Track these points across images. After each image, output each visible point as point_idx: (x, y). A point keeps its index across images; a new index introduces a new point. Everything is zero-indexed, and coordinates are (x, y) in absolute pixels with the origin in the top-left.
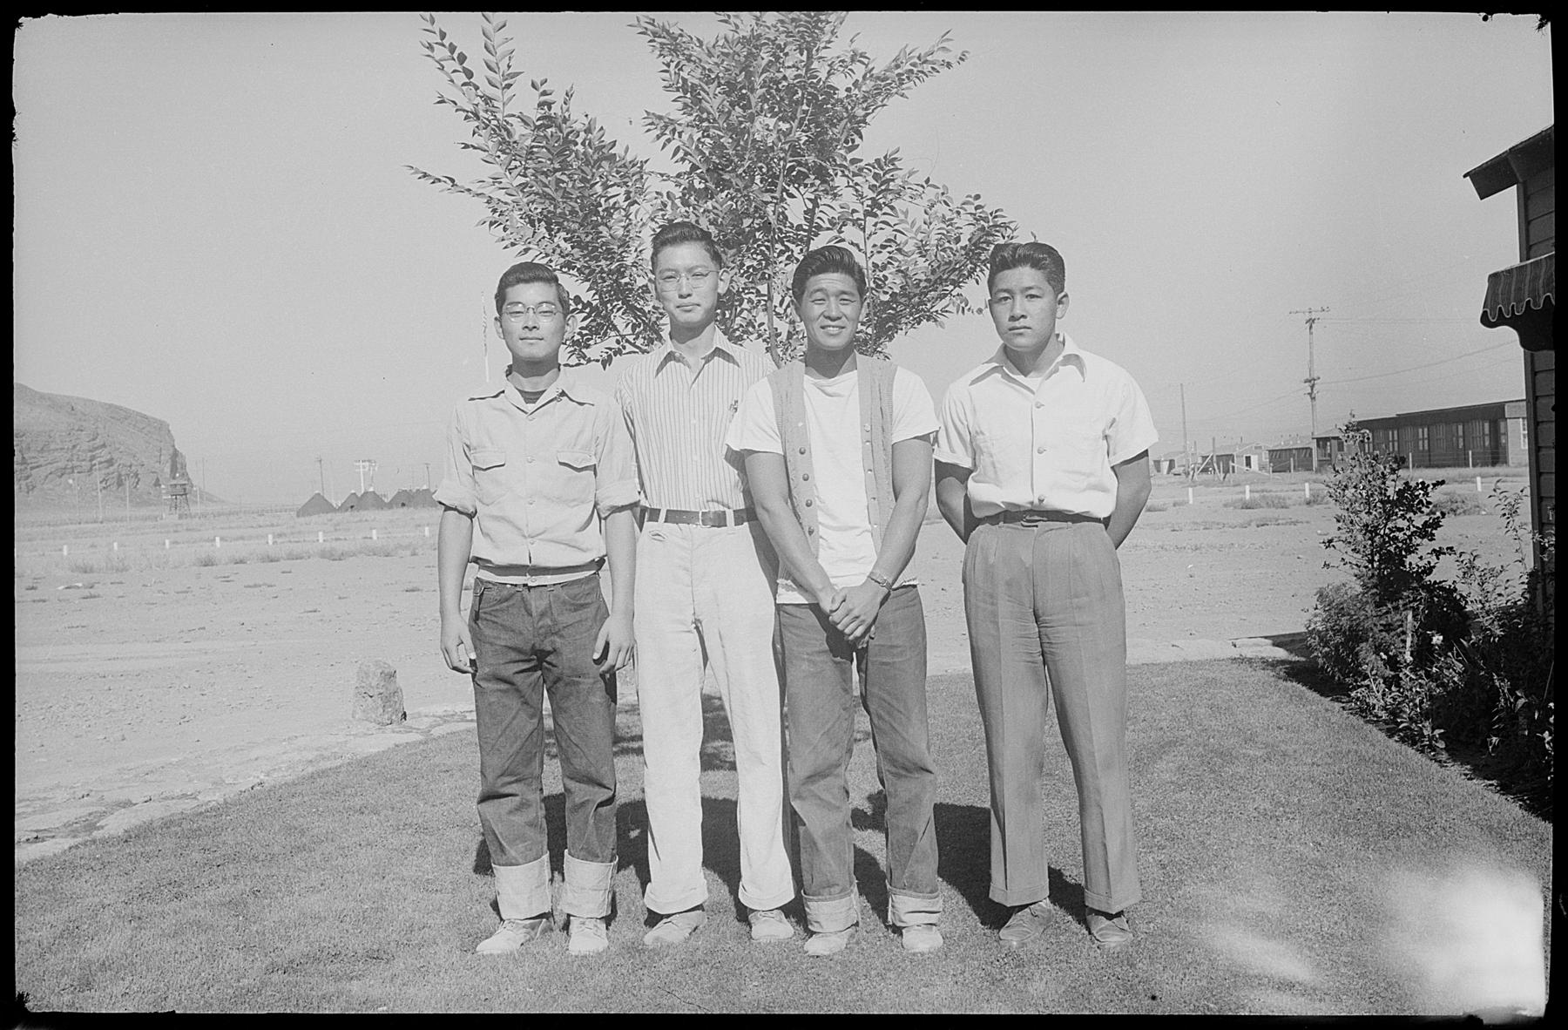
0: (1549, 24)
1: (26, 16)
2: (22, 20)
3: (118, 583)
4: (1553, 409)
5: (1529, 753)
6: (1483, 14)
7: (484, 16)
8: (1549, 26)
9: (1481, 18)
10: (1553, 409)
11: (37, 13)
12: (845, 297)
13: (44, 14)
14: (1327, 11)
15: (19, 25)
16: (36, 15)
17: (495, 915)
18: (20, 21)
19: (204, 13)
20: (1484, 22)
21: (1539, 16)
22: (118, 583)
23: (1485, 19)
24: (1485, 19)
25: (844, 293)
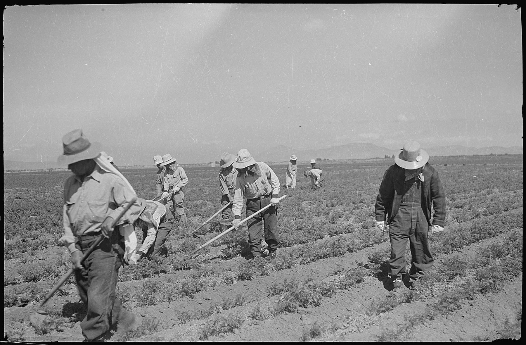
0: (520, 8)
1: (8, 5)
4: (523, 137)
10: (523, 137)
13: (14, 5)
16: (11, 5)
18: (5, 7)
23: (498, 6)
24: (498, 6)
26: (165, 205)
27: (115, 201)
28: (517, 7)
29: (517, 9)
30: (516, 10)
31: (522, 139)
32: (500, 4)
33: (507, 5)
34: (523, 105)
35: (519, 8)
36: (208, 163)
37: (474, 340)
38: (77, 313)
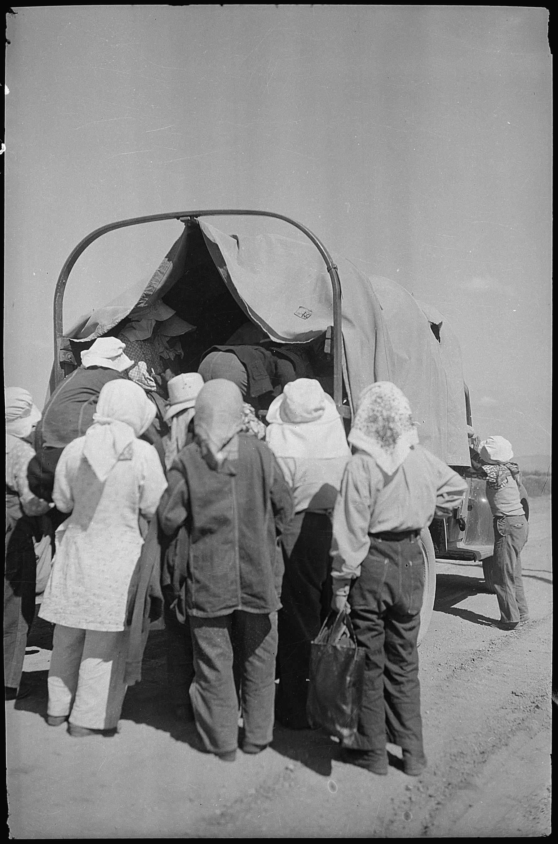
0: (12, 8)
4: (222, 5)
9: (9, 45)
10: (222, 5)
21: (7, 14)
23: (9, 43)
24: (9, 43)
28: (10, 13)
32: (6, 40)
35: (11, 10)
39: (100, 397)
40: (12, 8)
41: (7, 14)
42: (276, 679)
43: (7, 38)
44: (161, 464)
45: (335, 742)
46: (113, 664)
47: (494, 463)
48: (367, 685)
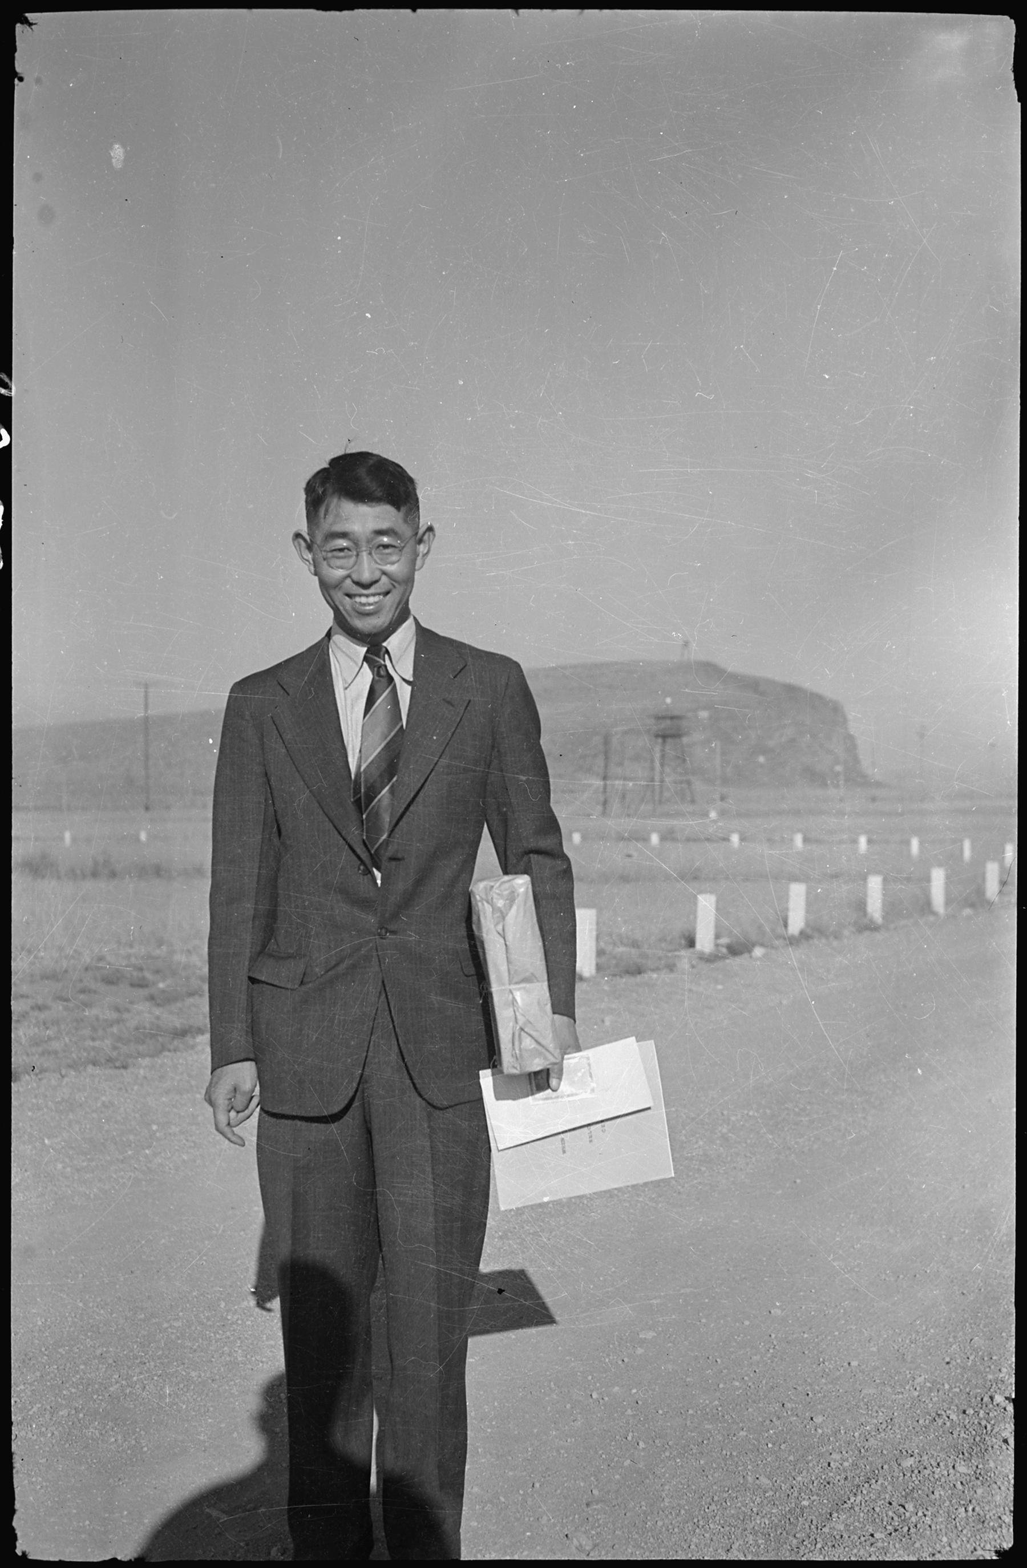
0: (27, 15)
1: (15, 1547)
2: (19, 1552)
3: (564, 1148)
4: (414, 10)
5: (18, 1090)
6: (16, 81)
7: (419, 570)
8: (30, 16)
9: (21, 84)
10: (414, 10)
11: (12, 1537)
12: (385, 540)
13: (13, 1529)
14: (13, 238)
15: (24, 1554)
16: (14, 1538)
17: (261, 985)
18: (20, 1554)
19: (12, 1224)
20: (25, 80)
21: (18, 25)
22: (564, 1148)
23: (21, 79)
24: (21, 79)
25: (380, 533)
26: (554, 1013)
27: (363, 664)
28: (22, 23)
29: (30, 24)
30: (33, 27)
31: (420, 11)
32: (15, 74)
33: (16, 54)
34: (318, 9)
35: (26, 19)
36: (367, 675)
37: (16, 1073)
38: (487, 851)
39: (594, 955)
40: (27, 15)
41: (18, 25)
42: (506, 811)
43: (18, 69)
44: (486, 946)
45: (921, 843)
46: (282, 1302)
47: (234, 1139)
48: (85, 962)
